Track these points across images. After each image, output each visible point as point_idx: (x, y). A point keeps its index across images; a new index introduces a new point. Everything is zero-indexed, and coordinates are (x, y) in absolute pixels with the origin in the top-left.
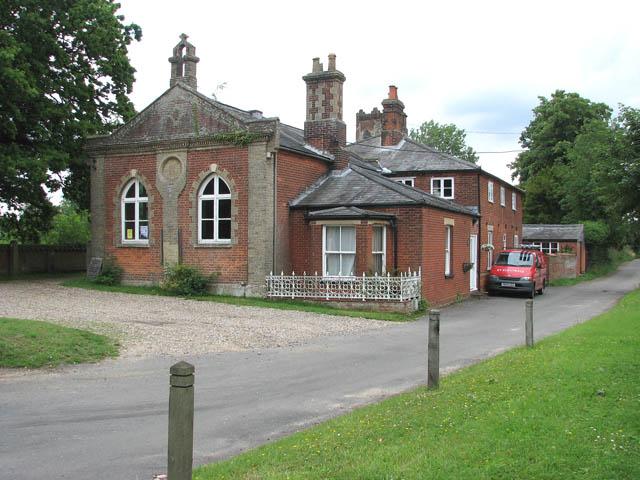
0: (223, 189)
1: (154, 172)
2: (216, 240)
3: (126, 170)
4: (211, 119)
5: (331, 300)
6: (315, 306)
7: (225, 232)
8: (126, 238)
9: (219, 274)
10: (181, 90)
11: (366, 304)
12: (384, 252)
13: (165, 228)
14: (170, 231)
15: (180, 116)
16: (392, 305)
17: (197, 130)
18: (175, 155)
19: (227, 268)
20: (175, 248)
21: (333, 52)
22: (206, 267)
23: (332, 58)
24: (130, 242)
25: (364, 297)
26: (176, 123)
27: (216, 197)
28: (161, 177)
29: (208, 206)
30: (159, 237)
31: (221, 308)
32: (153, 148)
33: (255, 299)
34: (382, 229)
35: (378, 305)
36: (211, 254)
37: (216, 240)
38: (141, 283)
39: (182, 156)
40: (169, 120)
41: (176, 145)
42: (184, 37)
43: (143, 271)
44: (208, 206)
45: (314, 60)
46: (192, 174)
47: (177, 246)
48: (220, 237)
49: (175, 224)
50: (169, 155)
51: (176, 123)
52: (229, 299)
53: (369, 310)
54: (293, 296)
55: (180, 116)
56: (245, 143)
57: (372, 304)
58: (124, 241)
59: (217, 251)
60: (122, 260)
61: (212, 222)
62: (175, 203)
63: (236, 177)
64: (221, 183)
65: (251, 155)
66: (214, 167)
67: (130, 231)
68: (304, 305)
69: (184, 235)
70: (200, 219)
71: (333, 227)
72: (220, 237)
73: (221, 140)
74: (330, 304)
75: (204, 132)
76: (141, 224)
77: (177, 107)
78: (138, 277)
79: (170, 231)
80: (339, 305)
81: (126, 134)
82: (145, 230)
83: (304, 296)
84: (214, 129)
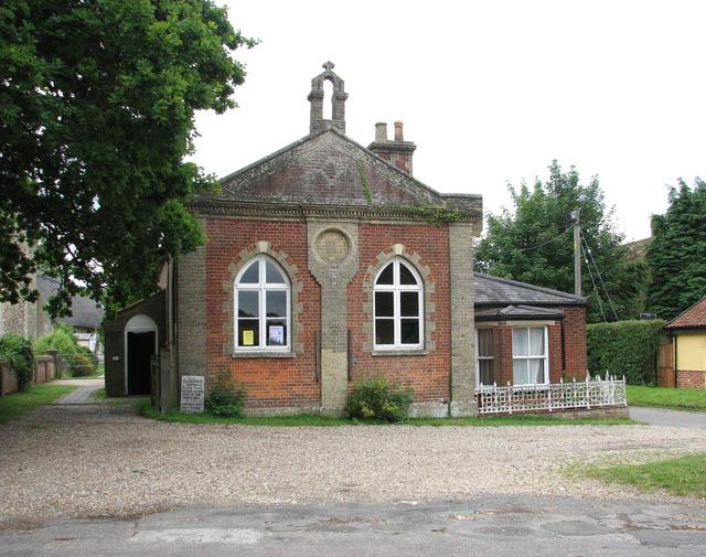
0: (407, 278)
1: (306, 247)
2: (398, 345)
3: (249, 242)
4: (388, 185)
5: (555, 411)
6: (537, 419)
7: (410, 333)
8: (241, 343)
9: (408, 390)
10: (337, 139)
11: (593, 412)
12: (547, 355)
13: (325, 330)
14: (334, 333)
15: (339, 173)
16: (618, 410)
17: (368, 197)
18: (338, 227)
19: (419, 380)
20: (342, 358)
21: (397, 120)
22: (387, 378)
23: (398, 126)
24: (248, 349)
25: (588, 405)
26: (331, 183)
27: (397, 288)
28: (316, 255)
29: (384, 302)
30: (313, 344)
31: (425, 431)
32: (302, 212)
33: (467, 418)
34: (543, 329)
35: (604, 412)
36: (397, 364)
37: (398, 345)
38: (278, 411)
39: (352, 231)
40: (319, 176)
41: (325, 212)
42: (329, 66)
43: (281, 394)
44: (384, 302)
45: (378, 125)
46: (367, 256)
47: (345, 354)
48: (403, 342)
49: (342, 323)
50: (329, 227)
51: (331, 183)
52: (418, 421)
53: (596, 418)
54: (510, 411)
55: (339, 173)
56: (445, 221)
57: (598, 411)
58: (238, 350)
59: (406, 360)
60: (240, 378)
61: (417, 320)
62: (342, 290)
63: (429, 264)
64: (403, 269)
65: (452, 238)
66: (399, 248)
67: (248, 336)
68: (530, 419)
69: (355, 338)
70: (421, 317)
71: (487, 330)
72: (403, 342)
73: (410, 214)
74: (554, 415)
75: (378, 200)
76: (269, 324)
77: (331, 160)
78: (270, 403)
79: (334, 333)
80: (565, 415)
81: (244, 187)
82: (276, 332)
83: (524, 409)
84: (395, 199)
